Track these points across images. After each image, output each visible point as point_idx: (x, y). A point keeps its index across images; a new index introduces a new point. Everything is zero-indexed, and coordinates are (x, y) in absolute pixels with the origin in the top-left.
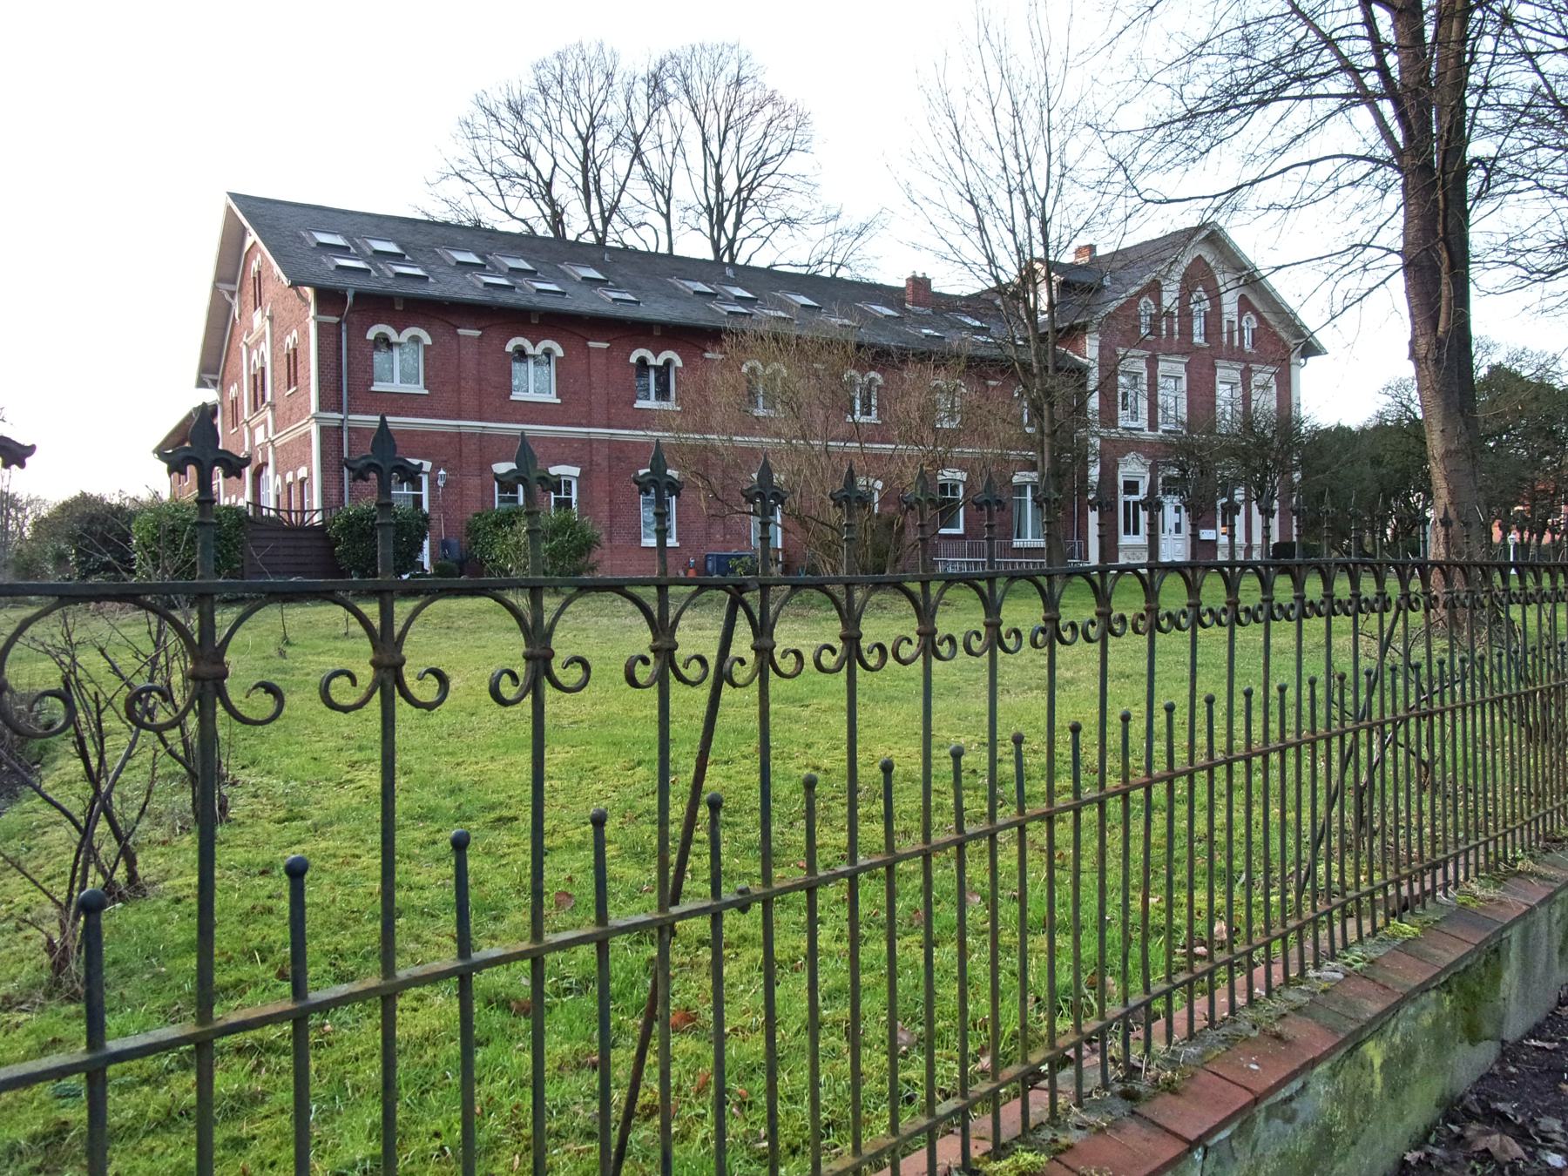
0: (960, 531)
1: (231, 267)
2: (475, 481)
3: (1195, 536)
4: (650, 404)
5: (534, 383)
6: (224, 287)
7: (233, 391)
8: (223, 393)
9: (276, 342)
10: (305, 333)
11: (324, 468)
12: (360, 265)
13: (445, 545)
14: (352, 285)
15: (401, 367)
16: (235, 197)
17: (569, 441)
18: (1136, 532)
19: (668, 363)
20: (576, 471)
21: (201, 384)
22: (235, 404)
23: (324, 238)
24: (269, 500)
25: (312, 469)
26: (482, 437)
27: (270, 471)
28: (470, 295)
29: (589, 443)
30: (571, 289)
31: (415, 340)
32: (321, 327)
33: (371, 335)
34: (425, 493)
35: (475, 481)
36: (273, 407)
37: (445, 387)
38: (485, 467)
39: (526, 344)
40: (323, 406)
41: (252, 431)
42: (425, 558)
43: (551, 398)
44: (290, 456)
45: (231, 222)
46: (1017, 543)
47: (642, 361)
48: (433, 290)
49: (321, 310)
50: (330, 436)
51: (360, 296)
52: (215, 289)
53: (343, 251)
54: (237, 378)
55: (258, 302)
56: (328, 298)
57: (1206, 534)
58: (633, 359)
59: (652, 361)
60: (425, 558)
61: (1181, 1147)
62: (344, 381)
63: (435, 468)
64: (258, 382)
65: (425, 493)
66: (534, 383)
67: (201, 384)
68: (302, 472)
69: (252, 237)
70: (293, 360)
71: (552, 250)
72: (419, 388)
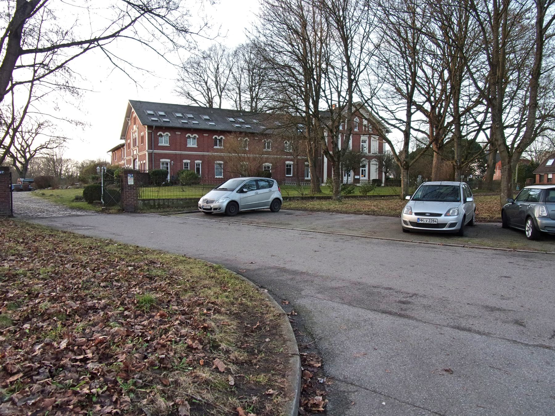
0: (291, 175)
1: (129, 115)
2: (179, 164)
3: (354, 177)
4: (218, 147)
5: (192, 144)
6: (127, 118)
7: (129, 141)
8: (126, 141)
9: (139, 134)
10: (145, 133)
11: (149, 161)
12: (156, 119)
13: (173, 177)
14: (154, 124)
15: (164, 140)
16: (130, 101)
17: (199, 155)
18: (365, 176)
19: (221, 138)
20: (201, 162)
21: (121, 139)
22: (129, 144)
23: (149, 112)
24: (137, 168)
25: (146, 161)
26: (181, 155)
27: (137, 160)
28: (179, 125)
29: (203, 156)
30: (201, 122)
31: (167, 135)
32: (148, 133)
33: (158, 134)
34: (169, 166)
35: (179, 164)
36: (138, 147)
37: (173, 145)
38: (181, 161)
39: (190, 135)
40: (149, 149)
41: (133, 151)
42: (169, 178)
43: (196, 146)
44: (142, 158)
45: (129, 106)
46: (306, 178)
47: (216, 138)
48: (170, 125)
49: (148, 129)
50: (150, 155)
51: (156, 127)
52: (125, 119)
53: (152, 115)
54: (130, 138)
55: (135, 124)
56: (150, 127)
57: (357, 177)
58: (214, 138)
59: (218, 138)
60: (169, 178)
61: (30, 84)
62: (153, 143)
63: (171, 161)
64: (135, 140)
65: (169, 166)
66: (192, 144)
67: (121, 139)
68: (144, 162)
69: (133, 110)
70: (143, 138)
71: (198, 111)
72: (168, 145)
